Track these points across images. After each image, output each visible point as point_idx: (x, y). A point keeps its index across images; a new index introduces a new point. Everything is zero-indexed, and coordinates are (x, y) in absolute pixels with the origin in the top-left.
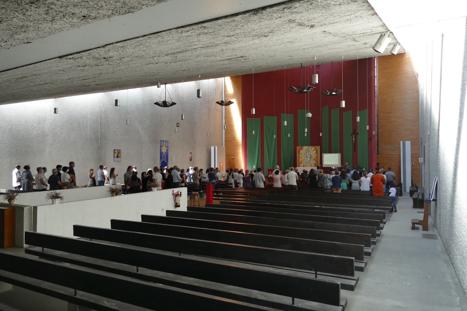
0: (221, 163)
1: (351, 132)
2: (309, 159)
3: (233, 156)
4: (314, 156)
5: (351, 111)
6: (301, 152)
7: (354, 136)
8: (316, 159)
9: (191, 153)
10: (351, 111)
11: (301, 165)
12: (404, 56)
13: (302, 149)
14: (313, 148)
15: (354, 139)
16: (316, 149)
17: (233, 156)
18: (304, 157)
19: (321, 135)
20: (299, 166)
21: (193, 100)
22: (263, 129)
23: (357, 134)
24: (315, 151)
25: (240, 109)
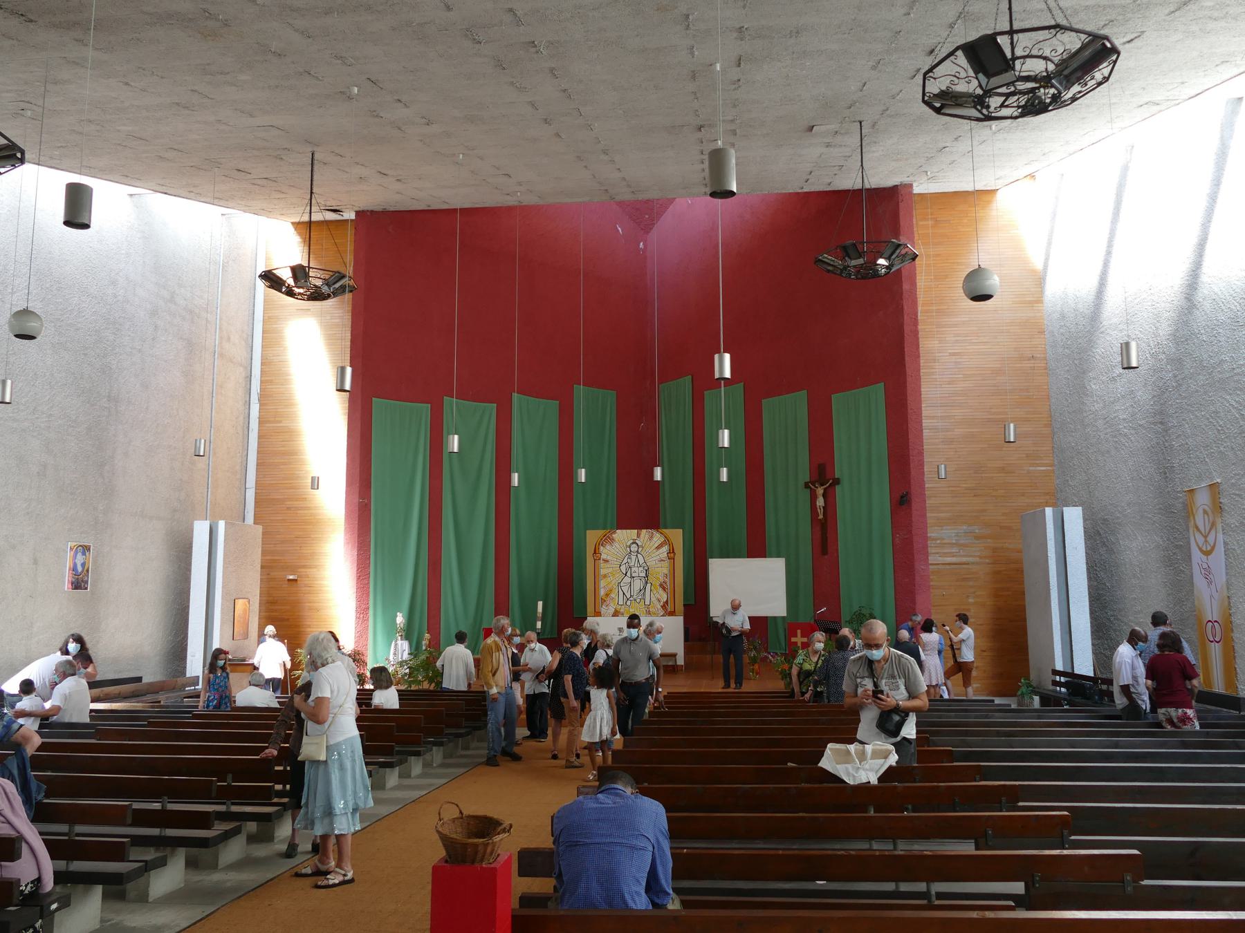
0: (240, 604)
1: (805, 476)
2: (638, 584)
3: (293, 569)
4: (661, 570)
5: (882, 385)
6: (605, 552)
7: (820, 491)
8: (669, 586)
9: (86, 549)
10: (882, 385)
11: (603, 610)
12: (989, 202)
13: (607, 539)
14: (658, 538)
15: (820, 502)
16: (667, 541)
17: (293, 569)
18: (619, 576)
19: (658, 474)
20: (598, 614)
21: (114, 283)
22: (478, 599)
23: (837, 482)
24: (665, 549)
25: (331, 340)
